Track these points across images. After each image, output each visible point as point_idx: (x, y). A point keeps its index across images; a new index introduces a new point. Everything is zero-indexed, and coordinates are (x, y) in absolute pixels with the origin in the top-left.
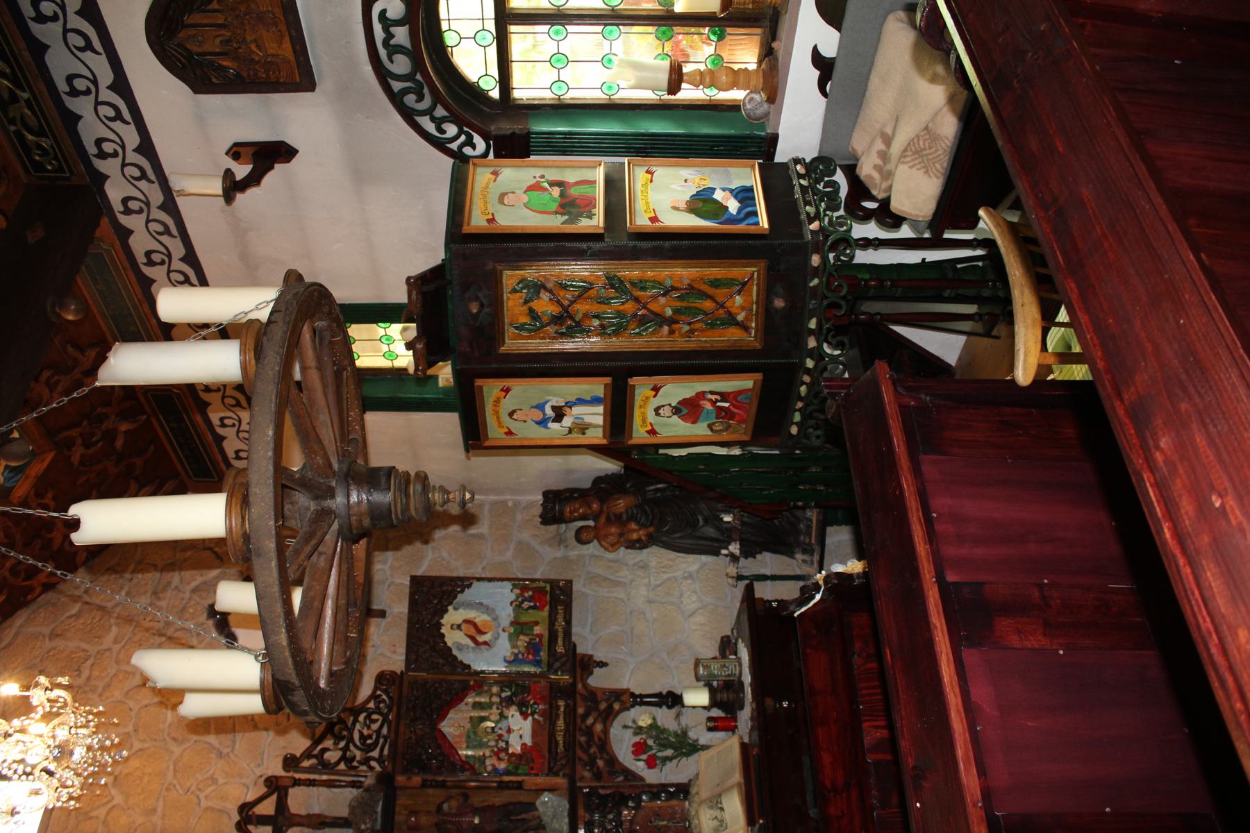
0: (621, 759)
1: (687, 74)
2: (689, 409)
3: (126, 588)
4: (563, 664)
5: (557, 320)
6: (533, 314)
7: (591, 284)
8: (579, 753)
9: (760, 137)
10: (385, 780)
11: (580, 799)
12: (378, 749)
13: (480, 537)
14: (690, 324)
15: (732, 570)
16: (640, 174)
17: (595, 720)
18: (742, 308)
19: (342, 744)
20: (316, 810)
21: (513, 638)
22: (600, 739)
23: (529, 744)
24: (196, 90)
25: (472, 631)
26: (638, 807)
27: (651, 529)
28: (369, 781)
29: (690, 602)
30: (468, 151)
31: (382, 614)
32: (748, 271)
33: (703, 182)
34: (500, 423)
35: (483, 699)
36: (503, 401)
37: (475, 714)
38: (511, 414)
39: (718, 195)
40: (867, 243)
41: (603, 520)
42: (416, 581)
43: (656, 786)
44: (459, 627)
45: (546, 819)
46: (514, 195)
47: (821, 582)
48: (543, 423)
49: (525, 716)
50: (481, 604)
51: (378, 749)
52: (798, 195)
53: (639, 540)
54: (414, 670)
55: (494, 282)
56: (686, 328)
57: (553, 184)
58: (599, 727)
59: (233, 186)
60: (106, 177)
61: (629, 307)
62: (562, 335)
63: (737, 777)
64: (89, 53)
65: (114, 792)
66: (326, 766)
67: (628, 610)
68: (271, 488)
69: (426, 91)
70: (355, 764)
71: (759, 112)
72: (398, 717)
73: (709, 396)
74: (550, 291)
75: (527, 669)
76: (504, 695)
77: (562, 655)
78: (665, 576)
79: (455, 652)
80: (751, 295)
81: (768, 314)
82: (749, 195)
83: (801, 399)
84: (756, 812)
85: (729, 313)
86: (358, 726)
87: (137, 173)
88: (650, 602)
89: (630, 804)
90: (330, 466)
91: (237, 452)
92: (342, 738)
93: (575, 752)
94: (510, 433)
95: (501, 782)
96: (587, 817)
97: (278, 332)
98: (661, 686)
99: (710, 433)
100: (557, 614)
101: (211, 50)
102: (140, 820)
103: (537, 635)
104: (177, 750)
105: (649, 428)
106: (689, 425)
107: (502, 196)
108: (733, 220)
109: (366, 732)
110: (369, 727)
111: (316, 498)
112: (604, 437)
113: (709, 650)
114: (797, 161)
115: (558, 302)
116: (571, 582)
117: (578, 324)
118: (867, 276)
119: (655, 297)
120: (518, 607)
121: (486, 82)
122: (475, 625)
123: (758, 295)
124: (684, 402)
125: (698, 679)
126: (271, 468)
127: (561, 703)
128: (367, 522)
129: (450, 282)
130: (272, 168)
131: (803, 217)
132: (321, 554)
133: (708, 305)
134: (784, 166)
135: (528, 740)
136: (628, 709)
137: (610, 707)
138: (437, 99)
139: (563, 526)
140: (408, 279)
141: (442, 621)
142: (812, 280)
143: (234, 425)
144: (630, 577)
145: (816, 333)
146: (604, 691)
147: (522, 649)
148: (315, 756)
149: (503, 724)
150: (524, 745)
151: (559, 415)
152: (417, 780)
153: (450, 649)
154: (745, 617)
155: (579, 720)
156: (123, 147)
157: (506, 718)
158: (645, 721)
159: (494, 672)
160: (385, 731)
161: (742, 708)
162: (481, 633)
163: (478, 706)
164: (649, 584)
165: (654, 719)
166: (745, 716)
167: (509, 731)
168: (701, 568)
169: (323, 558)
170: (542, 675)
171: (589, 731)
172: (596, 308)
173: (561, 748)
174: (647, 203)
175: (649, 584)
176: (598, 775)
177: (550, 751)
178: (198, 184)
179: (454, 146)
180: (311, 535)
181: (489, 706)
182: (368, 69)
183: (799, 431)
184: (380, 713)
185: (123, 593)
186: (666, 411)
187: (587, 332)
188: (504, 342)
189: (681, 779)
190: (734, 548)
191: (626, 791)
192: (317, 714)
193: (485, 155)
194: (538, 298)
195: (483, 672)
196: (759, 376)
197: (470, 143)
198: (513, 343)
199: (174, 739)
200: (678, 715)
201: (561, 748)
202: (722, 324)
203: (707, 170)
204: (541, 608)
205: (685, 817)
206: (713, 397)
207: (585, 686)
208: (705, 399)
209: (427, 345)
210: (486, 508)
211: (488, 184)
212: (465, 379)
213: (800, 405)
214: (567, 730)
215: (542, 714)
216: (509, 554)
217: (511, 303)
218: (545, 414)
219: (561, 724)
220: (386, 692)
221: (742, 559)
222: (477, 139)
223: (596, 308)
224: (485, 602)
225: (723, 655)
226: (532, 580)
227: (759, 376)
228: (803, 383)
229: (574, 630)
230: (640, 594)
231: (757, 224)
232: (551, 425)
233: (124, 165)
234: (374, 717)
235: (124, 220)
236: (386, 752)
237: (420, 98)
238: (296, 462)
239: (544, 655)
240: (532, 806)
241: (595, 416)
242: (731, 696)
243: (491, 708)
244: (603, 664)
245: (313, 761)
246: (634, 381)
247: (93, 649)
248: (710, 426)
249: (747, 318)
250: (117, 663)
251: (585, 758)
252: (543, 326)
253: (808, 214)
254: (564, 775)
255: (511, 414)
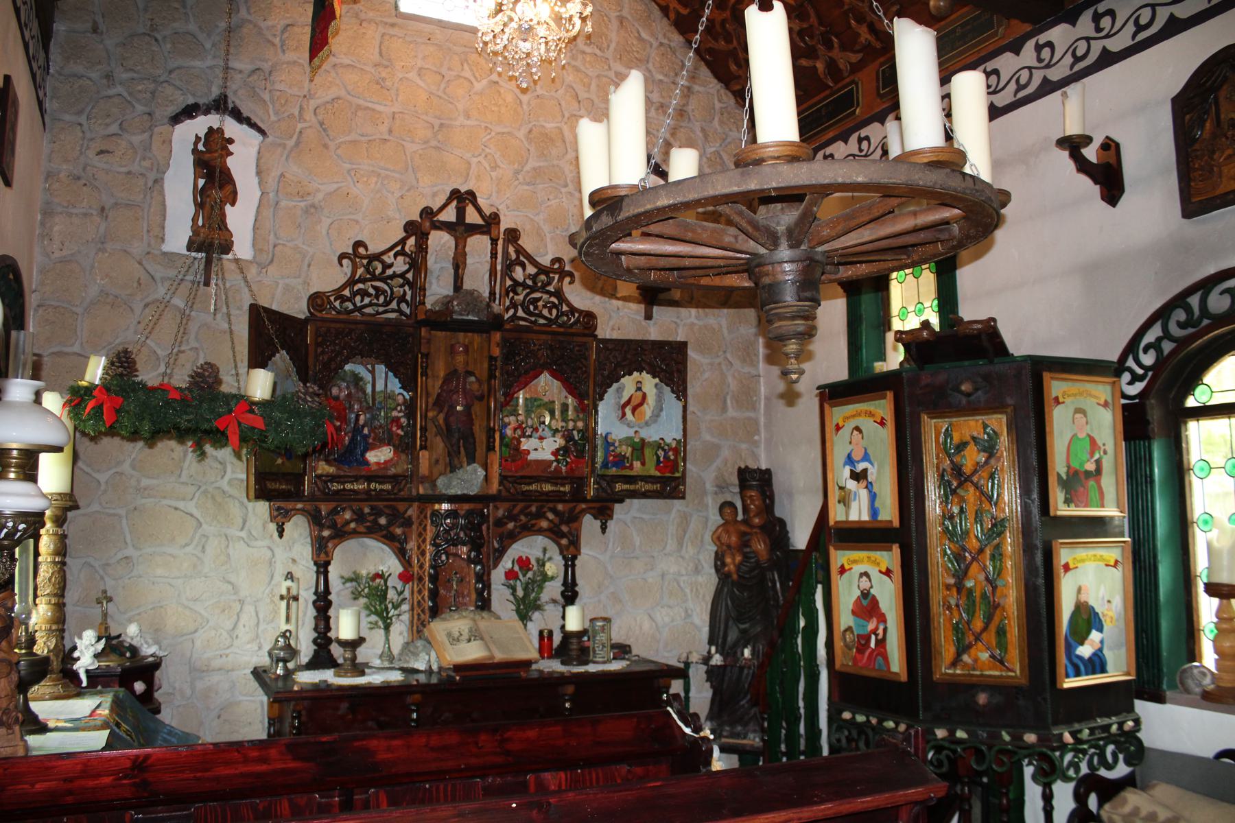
0: (514, 546)
1: (1230, 604)
2: (868, 607)
3: (666, 80)
4: (604, 490)
5: (957, 470)
6: (961, 446)
7: (996, 504)
8: (520, 506)
9: (1160, 683)
10: (496, 322)
11: (479, 506)
12: (524, 315)
13: (724, 409)
14: (957, 606)
15: (695, 658)
16: (1113, 554)
17: (551, 521)
18: (976, 660)
19: (529, 282)
20: (469, 261)
21: (628, 441)
22: (533, 525)
23: (529, 458)
24: (1175, 101)
25: (634, 402)
26: (470, 561)
27: (735, 576)
28: (497, 308)
29: (662, 616)
30: (1126, 377)
31: (649, 317)
32: (1015, 668)
33: (1108, 620)
34: (848, 418)
35: (571, 413)
36: (871, 420)
37: (557, 407)
38: (857, 429)
39: (1095, 636)
40: (1048, 798)
41: (743, 528)
42: (682, 347)
43: (489, 579)
44: (639, 389)
45: (460, 473)
46: (1084, 423)
47: (702, 734)
48: (850, 460)
49: (555, 453)
50: (661, 410)
51: (524, 315)
52: (1100, 721)
53: (724, 564)
54: (598, 346)
55: (994, 407)
56: (953, 602)
57: (1098, 463)
58: (544, 524)
59: (1073, 145)
60: (1074, 24)
61: (973, 544)
62: (941, 476)
63: (499, 656)
64: (1134, 29)
65: (485, 82)
66: (509, 267)
67: (655, 554)
68: (807, 183)
69: (1190, 330)
70: (511, 295)
71: (1190, 683)
72: (554, 333)
73: (881, 627)
74: (986, 462)
75: (600, 455)
76: (575, 433)
77: (613, 488)
78: (688, 591)
79: (615, 386)
80: (990, 669)
81: (967, 687)
82: (1098, 668)
83: (880, 722)
84: (467, 674)
85: (970, 646)
86: (545, 296)
87: (1079, 53)
88: (663, 576)
89: (473, 554)
90: (821, 244)
91: (867, 138)
92: (535, 282)
93: (522, 501)
94: (838, 428)
95: (494, 431)
96: (462, 513)
97: (955, 183)
98: (582, 586)
99: (842, 628)
100: (653, 483)
101: (1222, 110)
102: (460, 107)
103: (632, 465)
104: (521, 134)
105: (847, 567)
106: (851, 607)
107: (1082, 411)
108: (1070, 650)
109: (540, 304)
110: (544, 306)
111: (790, 232)
112: (836, 522)
113: (618, 634)
114: (1137, 722)
115: (975, 472)
116: (683, 498)
117: (954, 492)
118: (1011, 796)
119: (984, 568)
120: (658, 446)
121: (1203, 393)
122: (641, 404)
123: (990, 676)
124: (874, 602)
125: (592, 620)
126: (827, 181)
127: (567, 488)
128: (766, 280)
129: (991, 362)
130: (1096, 183)
131: (1077, 726)
132: (736, 237)
133: (978, 624)
134: (1131, 709)
135: (533, 456)
136: (561, 553)
137: (563, 535)
138: (1182, 343)
139: (737, 490)
140: (994, 320)
141: (644, 373)
142: (1008, 733)
143: (861, 150)
144: (687, 557)
145: (952, 738)
146: (578, 530)
147: (618, 450)
148: (518, 257)
149: (547, 433)
150: (528, 452)
151: (858, 476)
152: (496, 352)
153: (617, 381)
154: (653, 667)
155: (551, 505)
156: (1107, 36)
157: (554, 436)
158: (550, 569)
159: (596, 423)
160: (542, 321)
161: (563, 663)
162: (634, 411)
163: (565, 407)
164: (680, 575)
165: (552, 578)
166: (555, 666)
167: (541, 438)
168: (696, 627)
169: (732, 240)
170: (593, 469)
171: (540, 515)
172: (970, 509)
173: (525, 488)
174: (1083, 561)
175: (680, 575)
176: (499, 523)
177: (522, 477)
178: (1071, 111)
179: (1130, 363)
180: (756, 227)
181: (565, 420)
182: (1212, 270)
183: (846, 721)
184: (557, 317)
185: (661, 77)
186: (865, 583)
187: (945, 501)
188: (932, 418)
189: (495, 604)
190: (717, 660)
191: (484, 550)
192: (587, 239)
193: (1124, 396)
194: (979, 451)
195: (597, 412)
196: (904, 678)
197: (1135, 378)
198: (933, 429)
199: (530, 131)
200: (554, 601)
201: (525, 488)
202: (958, 640)
203: (1122, 624)
204: (657, 467)
205: (459, 607)
206: (880, 631)
207: (584, 512)
208: (878, 622)
209: (927, 341)
210: (752, 414)
211: (1096, 397)
212: (889, 381)
213: (874, 721)
214: (542, 493)
215: (558, 470)
216: (707, 437)
217: (972, 423)
218: (858, 462)
219: (548, 487)
220: (577, 321)
221: (705, 668)
222: (1139, 387)
223: (970, 509)
224: (663, 414)
225: (613, 646)
226: (684, 460)
227: (904, 678)
228: (897, 724)
229: (636, 501)
230: (670, 566)
231: (1067, 676)
232: (847, 469)
233: (1088, 39)
234: (554, 312)
235: (1030, 46)
236: (522, 323)
237: (1181, 325)
238: (828, 209)
239: (613, 471)
240: (471, 459)
241: (858, 512)
242: (574, 653)
243: (563, 420)
244: (604, 529)
245: (514, 256)
246: (896, 549)
247: (609, 54)
248: (849, 629)
249: (966, 665)
250: (598, 76)
251: (516, 511)
252: (949, 455)
253: (1080, 731)
254: (499, 491)
255: (857, 429)
